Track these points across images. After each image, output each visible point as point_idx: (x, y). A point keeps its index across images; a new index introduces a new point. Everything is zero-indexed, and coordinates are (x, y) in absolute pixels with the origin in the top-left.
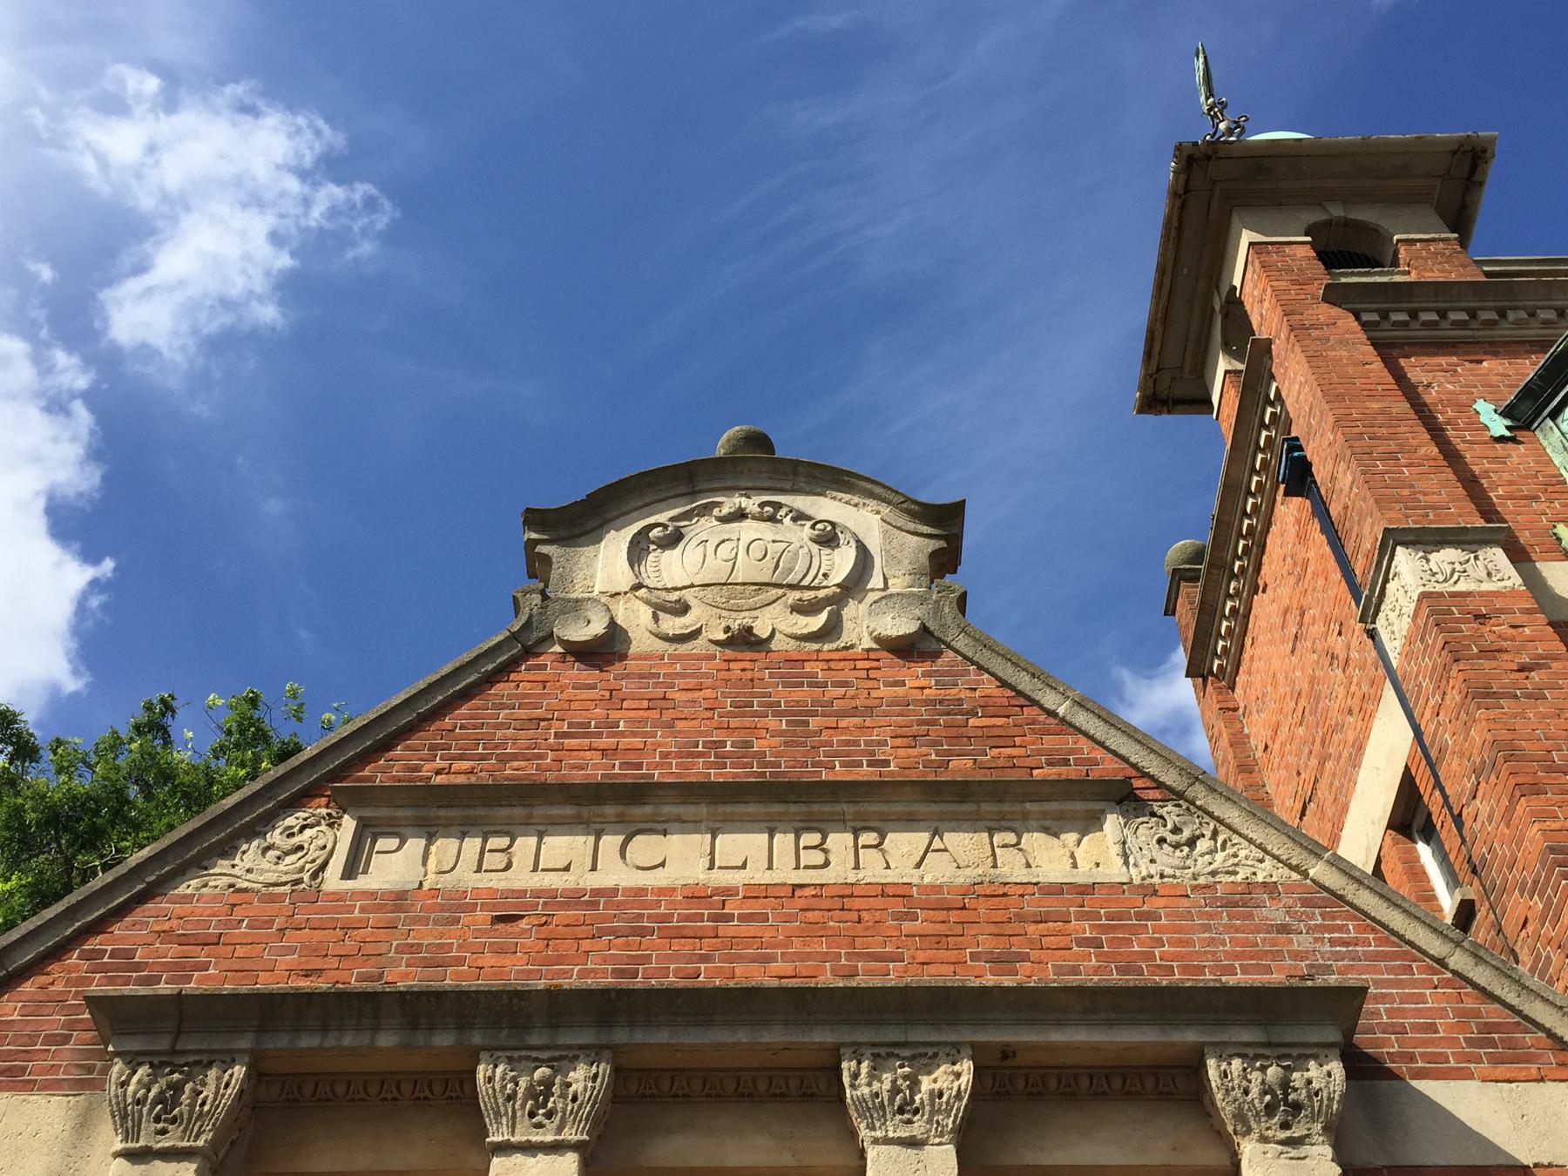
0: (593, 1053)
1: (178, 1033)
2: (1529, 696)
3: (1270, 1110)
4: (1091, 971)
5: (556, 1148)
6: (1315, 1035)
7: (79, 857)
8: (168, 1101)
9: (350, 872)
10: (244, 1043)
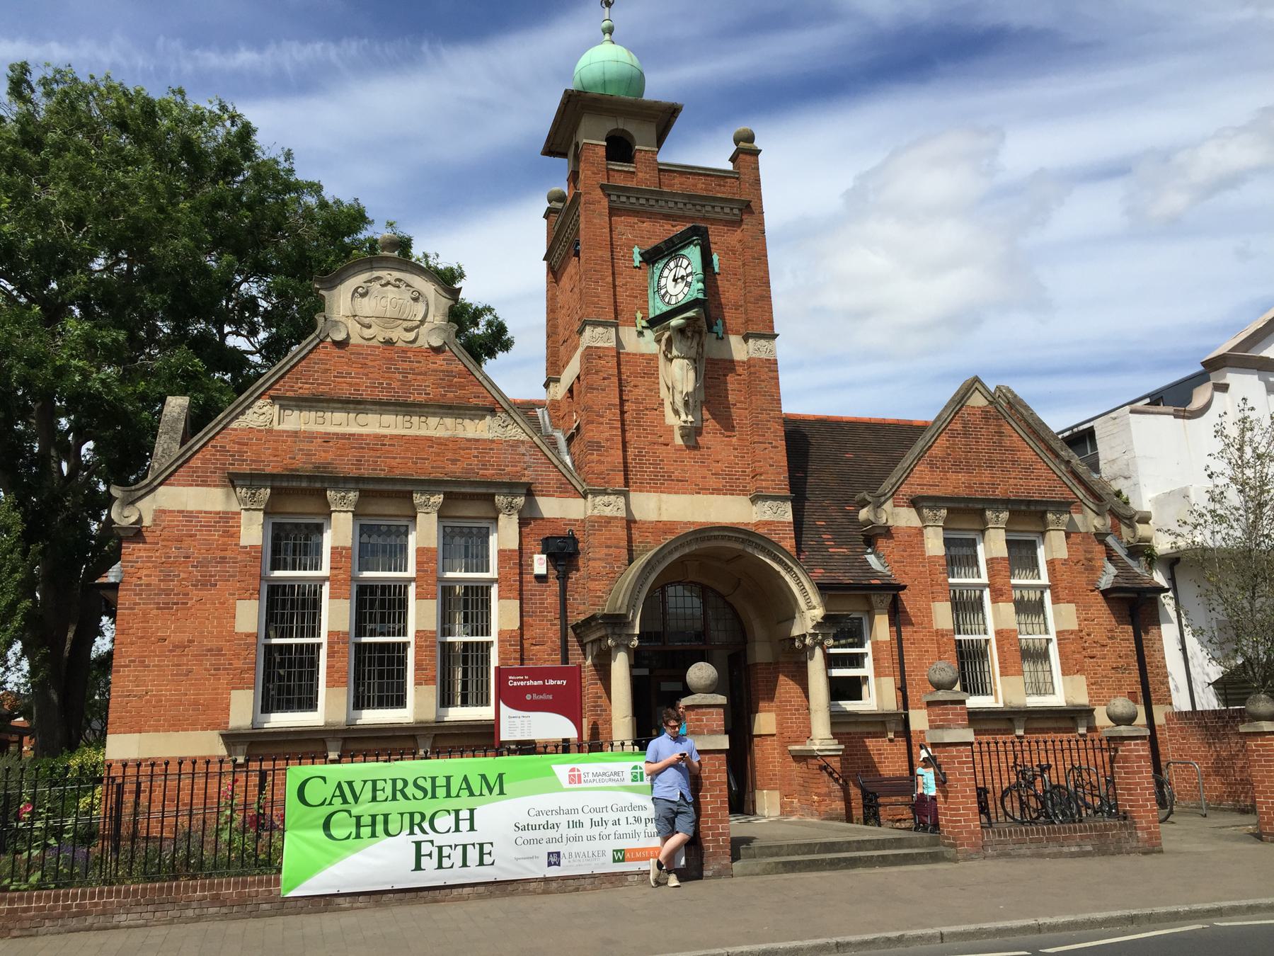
2: (602, 389)
3: (507, 508)
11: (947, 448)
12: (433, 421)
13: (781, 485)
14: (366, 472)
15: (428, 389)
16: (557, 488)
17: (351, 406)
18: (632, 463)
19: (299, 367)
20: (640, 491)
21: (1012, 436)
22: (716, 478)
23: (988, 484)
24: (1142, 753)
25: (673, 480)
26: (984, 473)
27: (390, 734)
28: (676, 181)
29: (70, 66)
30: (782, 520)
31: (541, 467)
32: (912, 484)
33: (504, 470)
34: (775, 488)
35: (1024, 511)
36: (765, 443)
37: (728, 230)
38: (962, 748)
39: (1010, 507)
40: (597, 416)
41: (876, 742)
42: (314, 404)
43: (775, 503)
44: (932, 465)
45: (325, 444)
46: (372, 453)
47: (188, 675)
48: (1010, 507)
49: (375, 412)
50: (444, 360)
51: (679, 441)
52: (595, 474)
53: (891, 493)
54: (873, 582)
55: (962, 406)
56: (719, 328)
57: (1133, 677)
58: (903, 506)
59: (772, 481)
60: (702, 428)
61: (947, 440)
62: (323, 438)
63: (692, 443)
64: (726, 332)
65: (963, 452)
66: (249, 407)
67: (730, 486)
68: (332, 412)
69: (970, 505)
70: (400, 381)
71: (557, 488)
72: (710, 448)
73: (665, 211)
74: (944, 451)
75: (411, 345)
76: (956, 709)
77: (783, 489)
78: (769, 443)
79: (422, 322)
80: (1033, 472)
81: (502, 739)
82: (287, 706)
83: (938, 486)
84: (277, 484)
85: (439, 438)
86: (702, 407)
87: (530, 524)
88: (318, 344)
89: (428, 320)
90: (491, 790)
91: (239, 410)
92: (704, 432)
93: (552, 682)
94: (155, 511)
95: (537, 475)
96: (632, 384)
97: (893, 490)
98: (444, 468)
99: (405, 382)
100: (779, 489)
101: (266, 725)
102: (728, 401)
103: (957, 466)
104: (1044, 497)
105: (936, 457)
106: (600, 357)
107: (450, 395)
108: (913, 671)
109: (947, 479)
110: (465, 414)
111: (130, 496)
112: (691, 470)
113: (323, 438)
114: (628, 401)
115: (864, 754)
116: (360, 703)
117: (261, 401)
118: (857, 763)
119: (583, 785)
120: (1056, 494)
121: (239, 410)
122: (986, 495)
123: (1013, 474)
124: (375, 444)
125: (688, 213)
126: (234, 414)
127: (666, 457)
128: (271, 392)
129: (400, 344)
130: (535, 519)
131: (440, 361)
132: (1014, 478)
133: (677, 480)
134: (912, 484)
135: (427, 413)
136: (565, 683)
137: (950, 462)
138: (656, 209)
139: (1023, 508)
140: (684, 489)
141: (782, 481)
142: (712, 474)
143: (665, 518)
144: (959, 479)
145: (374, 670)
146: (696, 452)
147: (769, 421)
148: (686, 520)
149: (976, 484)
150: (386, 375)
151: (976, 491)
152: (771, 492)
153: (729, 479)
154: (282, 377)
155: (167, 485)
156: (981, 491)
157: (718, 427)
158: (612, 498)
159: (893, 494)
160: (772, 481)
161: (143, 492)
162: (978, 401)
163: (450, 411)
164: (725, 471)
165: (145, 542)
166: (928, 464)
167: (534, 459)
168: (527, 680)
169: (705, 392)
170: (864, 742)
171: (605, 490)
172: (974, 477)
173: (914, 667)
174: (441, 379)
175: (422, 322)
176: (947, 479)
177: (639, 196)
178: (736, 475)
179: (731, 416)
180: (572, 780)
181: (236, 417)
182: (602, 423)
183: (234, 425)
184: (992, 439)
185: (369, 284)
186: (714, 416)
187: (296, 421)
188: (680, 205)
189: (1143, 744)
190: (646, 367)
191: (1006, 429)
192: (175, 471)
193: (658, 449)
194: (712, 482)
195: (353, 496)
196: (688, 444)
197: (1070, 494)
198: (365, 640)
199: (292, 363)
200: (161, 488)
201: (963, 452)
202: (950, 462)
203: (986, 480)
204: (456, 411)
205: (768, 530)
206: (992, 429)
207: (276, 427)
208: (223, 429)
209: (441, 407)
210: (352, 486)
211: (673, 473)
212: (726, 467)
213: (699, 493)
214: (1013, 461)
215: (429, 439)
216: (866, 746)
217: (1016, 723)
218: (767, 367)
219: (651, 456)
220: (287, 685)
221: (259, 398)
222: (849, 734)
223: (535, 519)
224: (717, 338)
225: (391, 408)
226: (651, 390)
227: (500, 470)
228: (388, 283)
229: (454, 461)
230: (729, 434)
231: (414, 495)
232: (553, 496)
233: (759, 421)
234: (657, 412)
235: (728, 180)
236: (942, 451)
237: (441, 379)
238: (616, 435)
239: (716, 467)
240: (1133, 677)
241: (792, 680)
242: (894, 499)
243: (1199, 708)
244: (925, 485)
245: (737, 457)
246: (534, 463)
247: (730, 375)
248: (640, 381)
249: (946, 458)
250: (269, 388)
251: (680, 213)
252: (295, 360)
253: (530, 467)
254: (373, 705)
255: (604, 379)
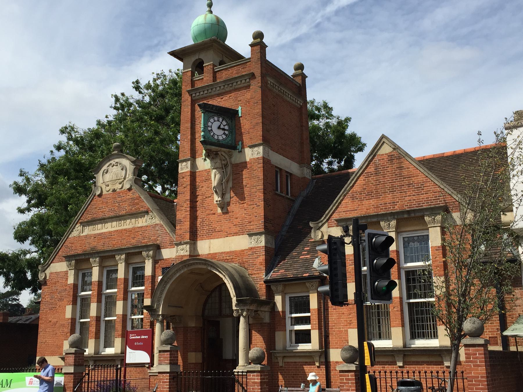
0: (98, 257)
1: (69, 258)
3: (147, 257)
4: (110, 248)
5: (97, 266)
6: (150, 249)
7: (41, 251)
8: (70, 264)
9: (82, 233)
10: (74, 259)
11: (364, 185)
12: (109, 224)
13: (260, 226)
14: (397, 208)
15: (126, 208)
16: (169, 244)
17: (102, 221)
18: (199, 226)
19: (88, 209)
20: (202, 240)
21: (409, 168)
22: (236, 227)
23: (390, 203)
24: (256, 381)
25: (216, 232)
26: (387, 197)
27: (106, 359)
28: (224, 74)
29: (162, 70)
30: (259, 245)
31: (163, 235)
32: (340, 212)
33: (150, 239)
34: (257, 229)
35: (407, 218)
36: (254, 205)
37: (247, 91)
38: (165, 375)
39: (396, 217)
40: (180, 207)
41: (310, 367)
42: (92, 223)
43: (256, 237)
44: (353, 198)
45: (95, 239)
46: (108, 240)
47: (56, 335)
48: (396, 217)
49: (110, 222)
50: (132, 193)
51: (219, 210)
52: (179, 235)
53: (325, 220)
54: (304, 275)
55: (375, 156)
56: (239, 147)
57: (495, 326)
58: (334, 226)
59: (255, 225)
60: (230, 202)
61: (364, 180)
62: (93, 236)
63: (225, 211)
64: (243, 147)
65: (374, 185)
66: (74, 228)
67: (242, 230)
68: (98, 225)
69: (369, 220)
70: (118, 206)
71: (169, 244)
72: (234, 212)
73: (217, 92)
74: (362, 187)
75: (121, 190)
76: (164, 355)
77: (261, 228)
78: (255, 204)
79: (125, 178)
80: (423, 189)
81: (127, 362)
82: (423, 336)
83: (356, 210)
84: (76, 258)
85: (129, 229)
86: (230, 191)
87: (159, 262)
88: (93, 198)
89: (127, 177)
90: (7, 385)
91: (71, 230)
92: (231, 204)
93: (143, 337)
94: (50, 273)
95: (162, 239)
96: (201, 186)
97: (327, 218)
98: (130, 242)
99: (119, 207)
100: (259, 229)
101: (412, 346)
102: (243, 184)
103: (370, 195)
104: (431, 205)
105: (356, 192)
106: (183, 177)
107: (133, 208)
108: (334, 326)
109: (363, 205)
110: (139, 216)
111: (43, 269)
112: (224, 225)
113: (93, 236)
114: (199, 195)
115: (302, 375)
116: (414, 336)
117: (78, 225)
118: (299, 379)
119: (32, 385)
120: (440, 201)
121: (71, 230)
122: (388, 211)
123: (408, 194)
124: (109, 236)
125: (227, 90)
126: (69, 232)
127: (214, 220)
128: (80, 221)
129: (118, 190)
130: (161, 260)
131: (130, 194)
132: (409, 196)
133: (218, 232)
134: (340, 212)
135: (126, 218)
136: (147, 337)
137: (365, 193)
138: (213, 93)
139: (406, 216)
140: (221, 235)
141: (261, 224)
142: (234, 225)
143: (212, 252)
144: (371, 203)
145: (425, 317)
146: (227, 215)
147: (256, 192)
148: (221, 251)
149: (382, 204)
150: (114, 205)
151: (381, 209)
152: (255, 231)
153: (242, 226)
154: (83, 214)
155: (54, 263)
156: (385, 209)
157: (238, 200)
158: (185, 246)
159: (328, 220)
160: (255, 225)
161: (46, 267)
162: (386, 149)
163: (133, 216)
164: (240, 222)
165: (47, 285)
166: (350, 198)
167: (162, 232)
168: (136, 336)
169: (232, 182)
170: (303, 367)
171: (181, 242)
172: (381, 200)
173: (335, 323)
174: (130, 202)
175: (125, 178)
176: (363, 205)
177: (204, 90)
178: (245, 224)
179: (244, 192)
180: (30, 383)
181: (71, 233)
182: (182, 210)
183: (70, 236)
184: (394, 173)
185: (109, 167)
186: (236, 194)
187: (88, 231)
188: (222, 87)
189: (257, 376)
190: (207, 176)
191: (405, 164)
192: (55, 257)
193: (210, 217)
194: (234, 230)
195: (97, 259)
196: (223, 212)
197: (451, 200)
198: (412, 301)
199: (85, 208)
200: (52, 264)
201: (374, 185)
202: (365, 193)
203: (388, 201)
204: (135, 215)
205: (252, 252)
206: (395, 166)
207: (81, 235)
208: (67, 239)
209: (129, 215)
210: (97, 255)
211: (216, 228)
212: (240, 220)
213: (227, 236)
214: (409, 185)
215: (125, 230)
216: (304, 370)
217: (397, 358)
218: (257, 162)
219: (207, 221)
220: (417, 325)
221: (77, 224)
222: (296, 362)
223: (161, 260)
224: (239, 152)
225: (115, 219)
226: (208, 187)
227: (149, 239)
228: (114, 165)
229: (134, 238)
230: (243, 202)
231: (116, 256)
232: (167, 248)
233: (252, 193)
234: (211, 198)
235: (248, 64)
236: (360, 187)
237: (130, 202)
238: (187, 215)
239: (236, 221)
240: (495, 326)
241: (258, 333)
242: (329, 223)
243: (519, 350)
244: (348, 211)
245: (245, 214)
246: (161, 233)
247: (245, 170)
248: (204, 184)
249: (362, 191)
250: (79, 219)
251: (224, 91)
252: (86, 206)
253: (160, 235)
254: (431, 337)
255: (184, 188)
